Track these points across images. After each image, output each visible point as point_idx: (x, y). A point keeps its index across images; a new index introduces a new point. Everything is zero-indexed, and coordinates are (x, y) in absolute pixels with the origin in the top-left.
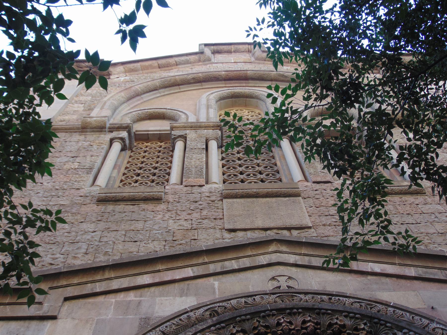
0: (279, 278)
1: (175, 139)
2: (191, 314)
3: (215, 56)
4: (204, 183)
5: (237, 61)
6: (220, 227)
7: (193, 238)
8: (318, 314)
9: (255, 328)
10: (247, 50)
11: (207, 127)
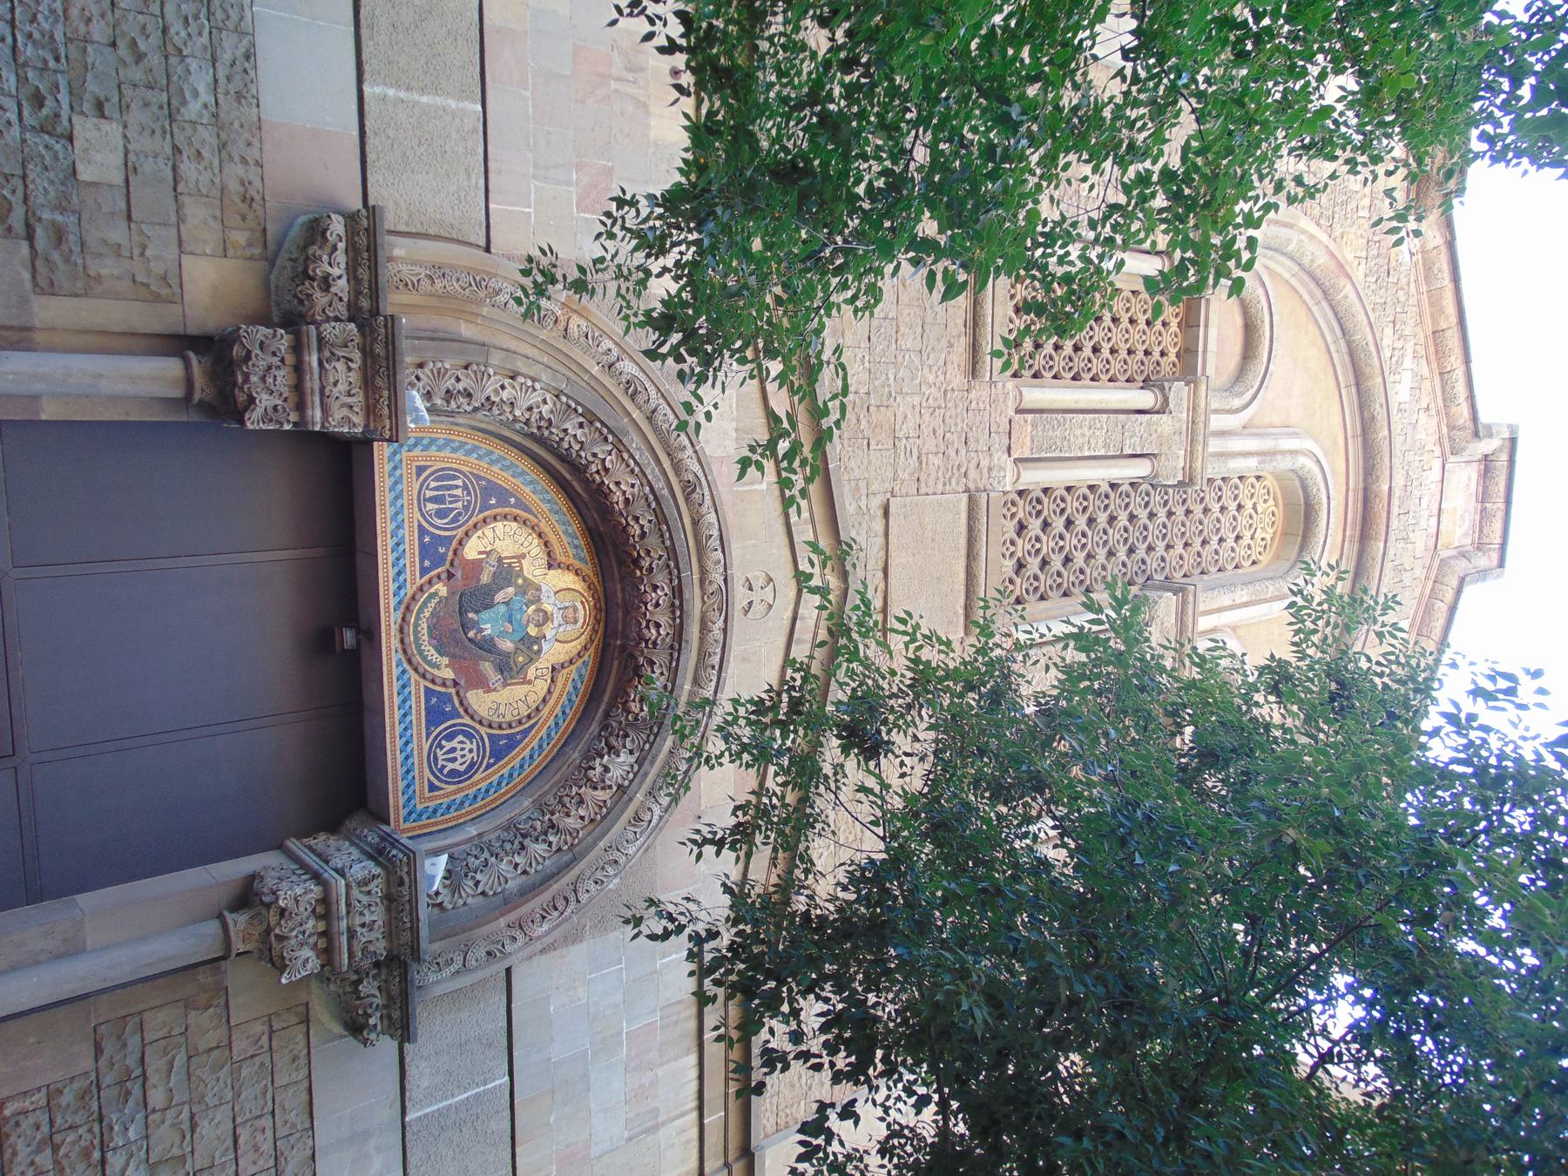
0: (770, 588)
1: (1162, 389)
2: (689, 451)
3: (1475, 465)
4: (1015, 455)
5: (1444, 516)
6: (897, 489)
7: (872, 442)
8: (672, 647)
9: (648, 552)
10: (1486, 540)
11: (1191, 455)
